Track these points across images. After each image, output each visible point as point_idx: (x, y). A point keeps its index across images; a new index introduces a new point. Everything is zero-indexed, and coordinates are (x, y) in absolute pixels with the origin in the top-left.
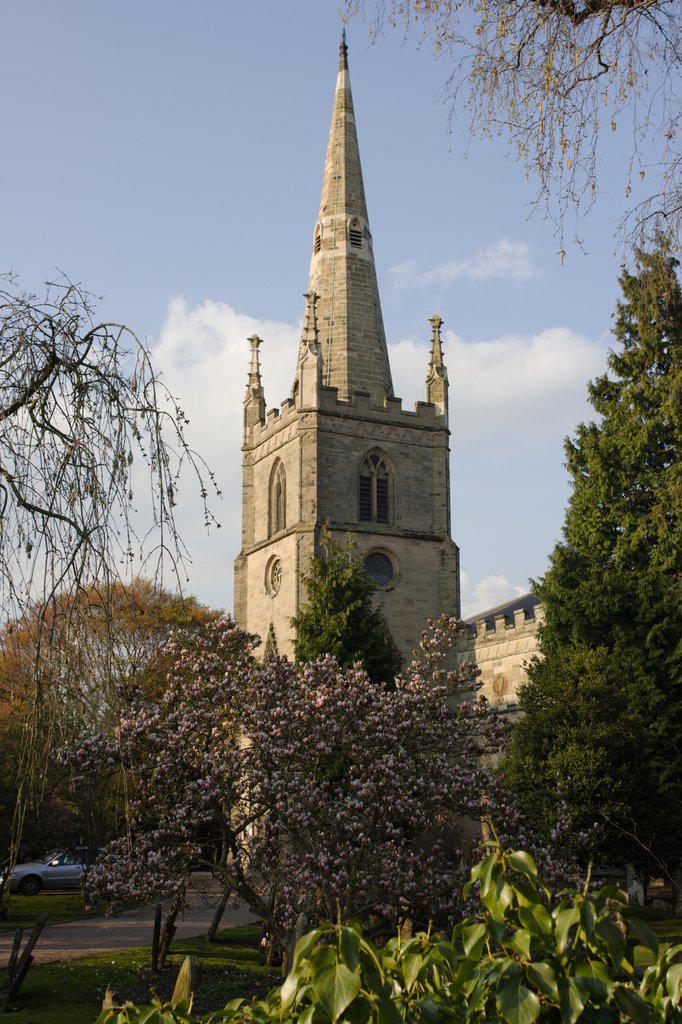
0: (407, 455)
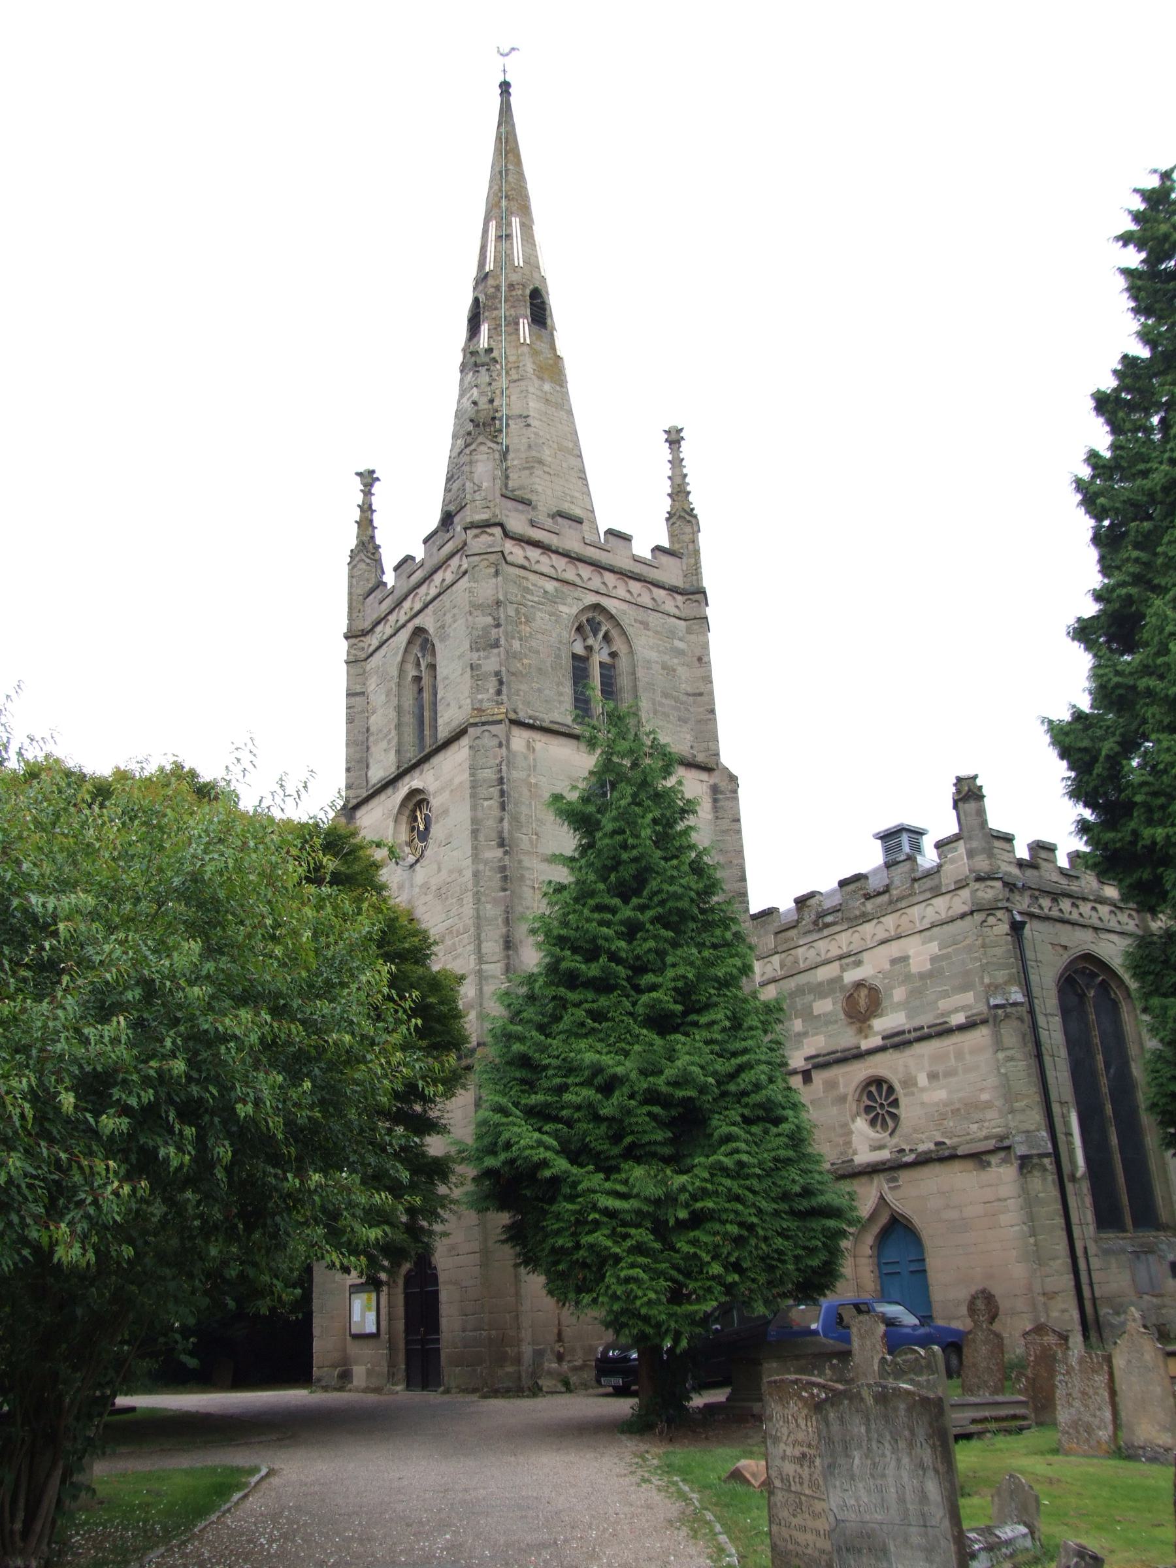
0: (646, 625)
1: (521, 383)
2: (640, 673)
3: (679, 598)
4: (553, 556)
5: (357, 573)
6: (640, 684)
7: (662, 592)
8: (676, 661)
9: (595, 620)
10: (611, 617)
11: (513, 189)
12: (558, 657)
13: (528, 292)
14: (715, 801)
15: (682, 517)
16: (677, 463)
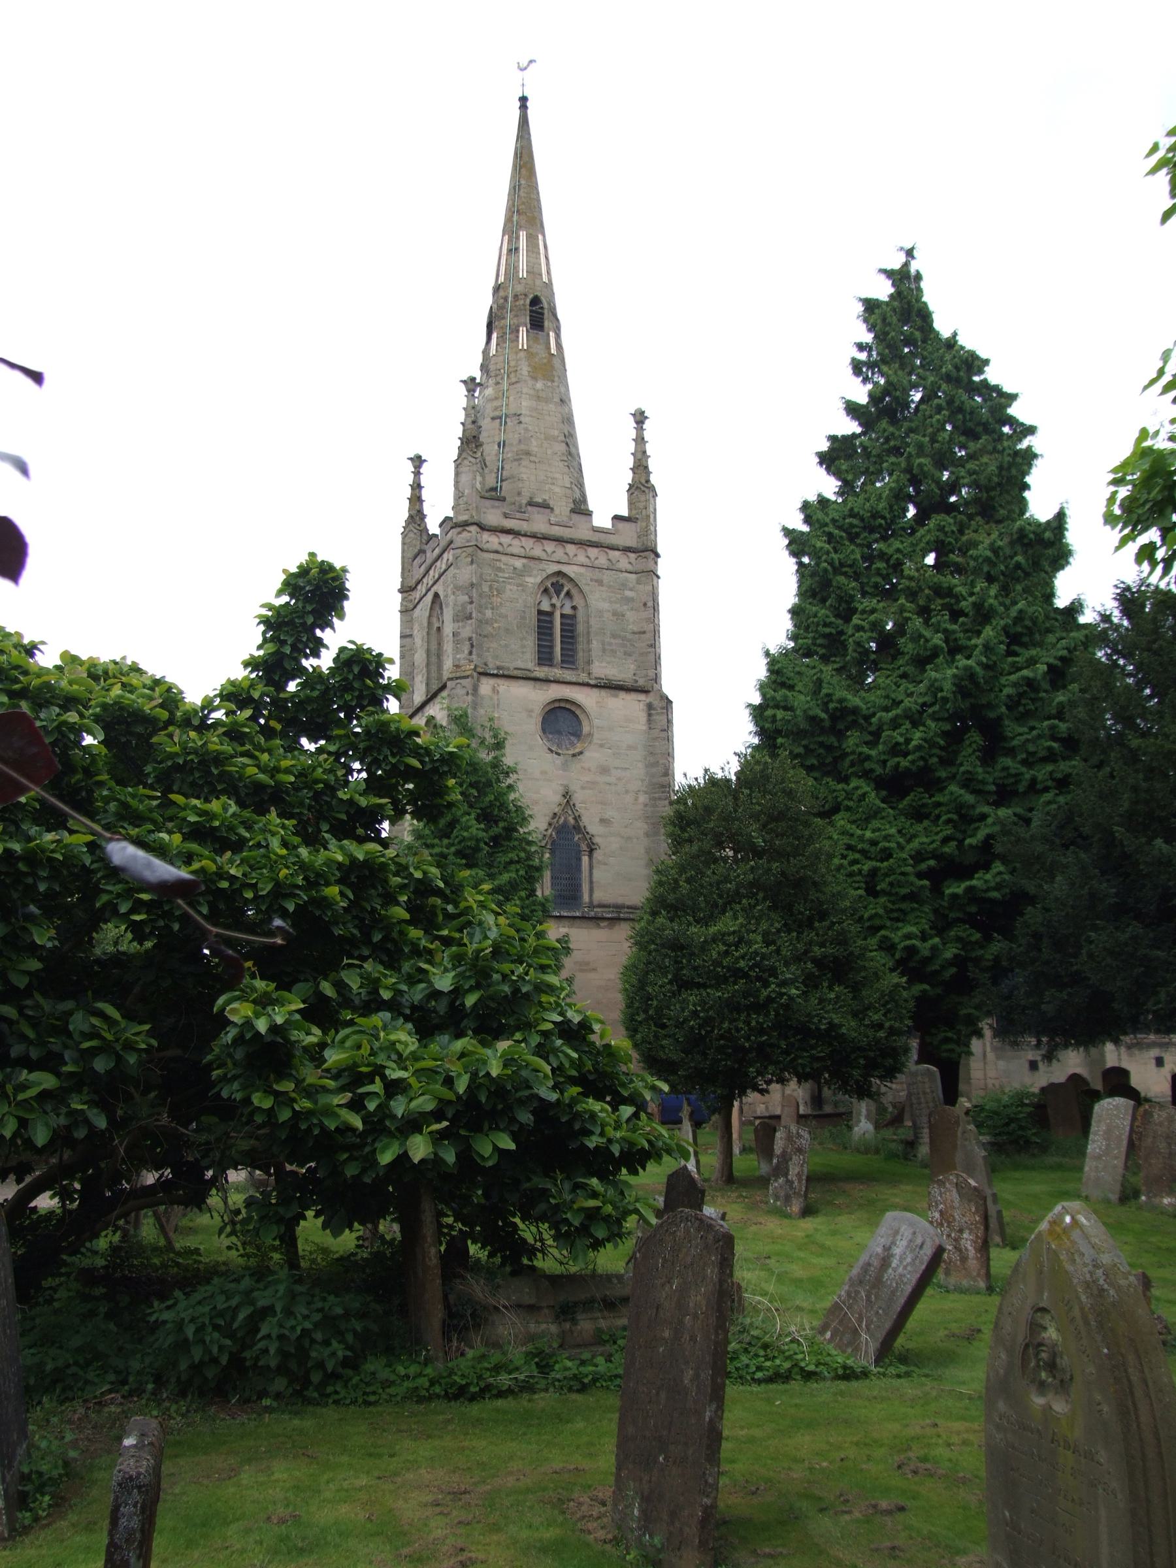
0: (600, 582)
1: (518, 385)
2: (593, 622)
3: (632, 555)
4: (523, 539)
5: (408, 540)
6: (592, 630)
7: (617, 553)
8: (625, 607)
9: (557, 584)
10: (571, 580)
11: (523, 203)
12: (523, 618)
13: (528, 301)
14: (650, 715)
15: (641, 487)
16: (640, 440)
